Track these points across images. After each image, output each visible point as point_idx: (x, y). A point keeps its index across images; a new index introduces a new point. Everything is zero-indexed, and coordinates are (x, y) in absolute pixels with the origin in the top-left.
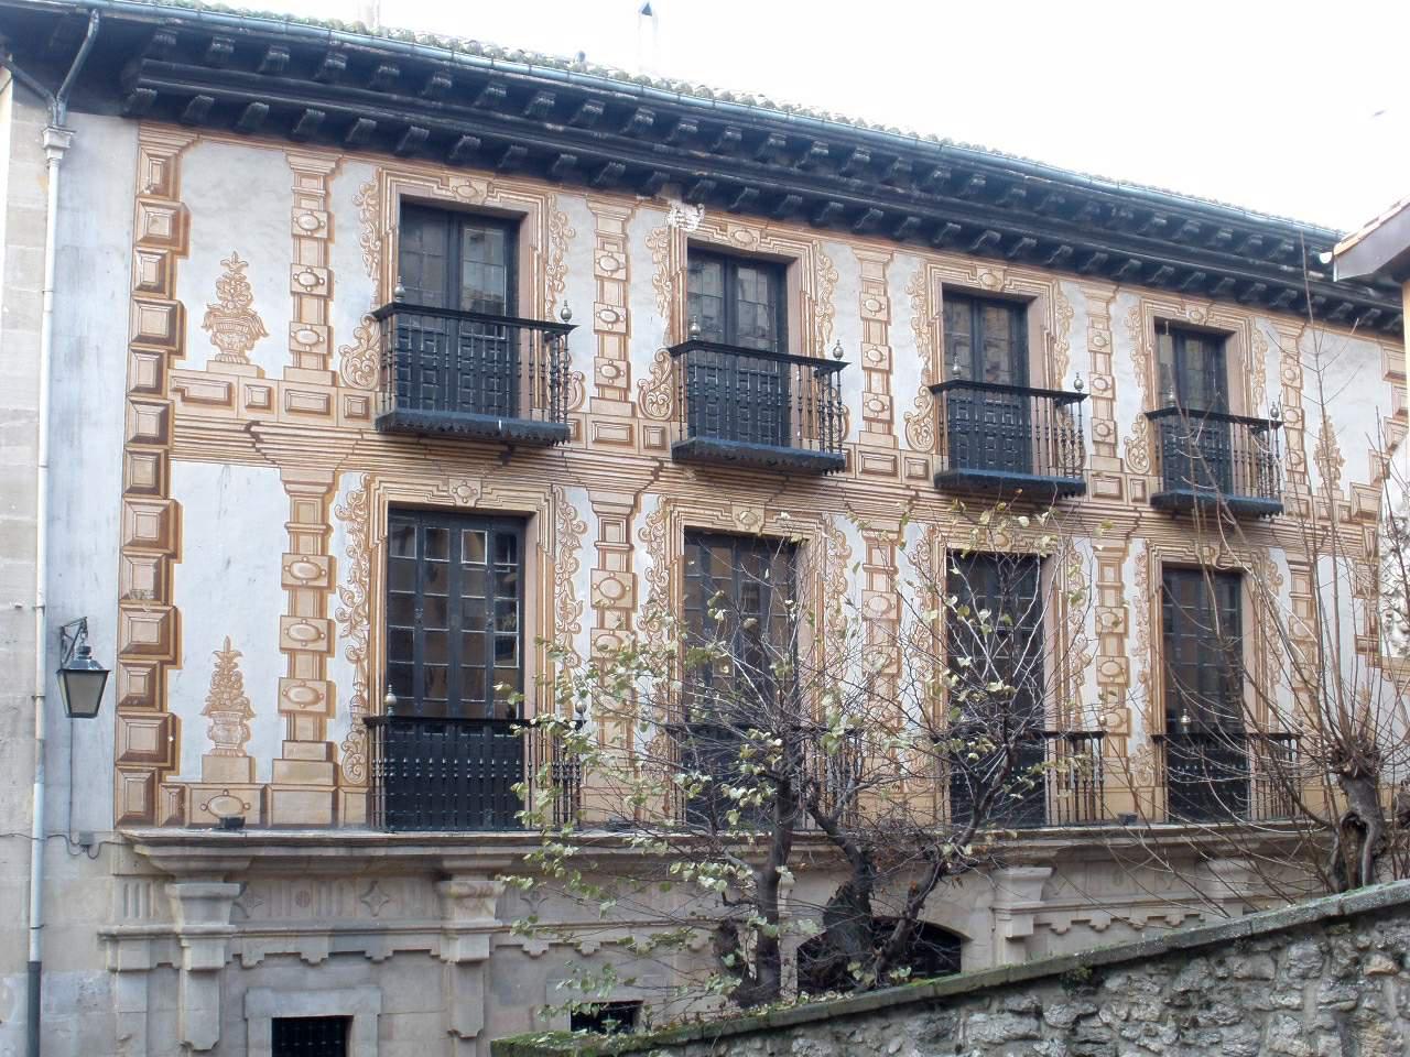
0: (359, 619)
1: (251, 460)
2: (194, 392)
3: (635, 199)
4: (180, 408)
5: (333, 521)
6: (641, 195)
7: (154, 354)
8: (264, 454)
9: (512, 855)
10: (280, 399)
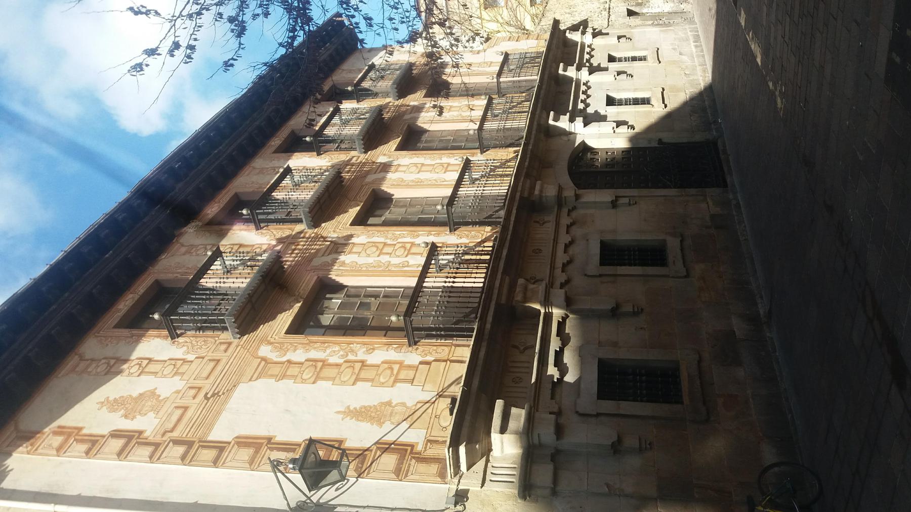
0: (349, 348)
1: (225, 402)
2: (171, 426)
3: (174, 243)
4: (175, 434)
5: (284, 359)
6: (173, 239)
7: (135, 445)
8: (227, 390)
9: (503, 273)
10: (199, 383)
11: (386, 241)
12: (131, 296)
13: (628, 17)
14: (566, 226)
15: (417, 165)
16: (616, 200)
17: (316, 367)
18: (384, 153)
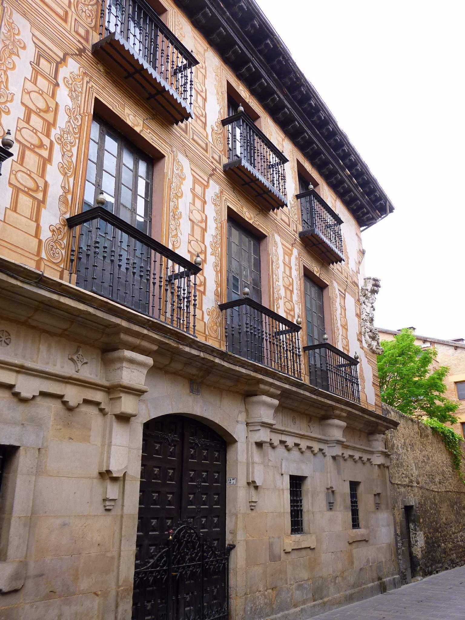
5: (60, 81)
11: (58, 128)
12: (248, 96)
13: (403, 507)
14: (62, 394)
15: (291, 286)
16: (115, 479)
17: (201, 222)
18: (224, 193)
